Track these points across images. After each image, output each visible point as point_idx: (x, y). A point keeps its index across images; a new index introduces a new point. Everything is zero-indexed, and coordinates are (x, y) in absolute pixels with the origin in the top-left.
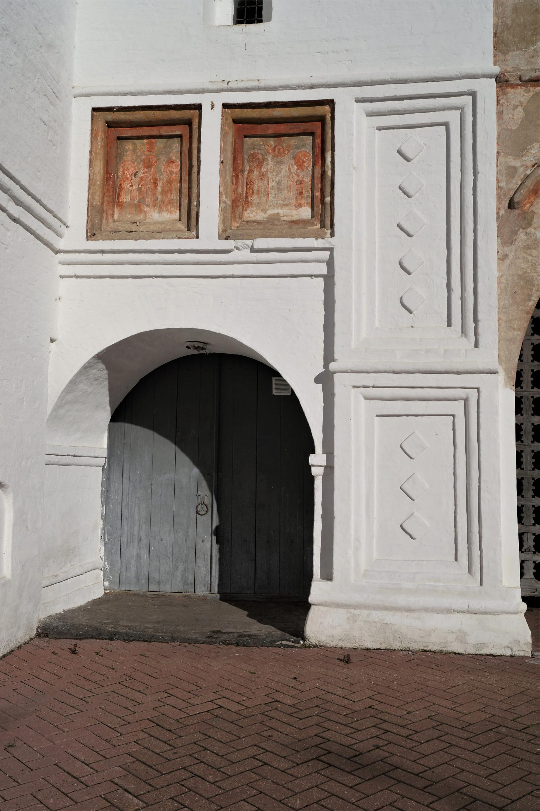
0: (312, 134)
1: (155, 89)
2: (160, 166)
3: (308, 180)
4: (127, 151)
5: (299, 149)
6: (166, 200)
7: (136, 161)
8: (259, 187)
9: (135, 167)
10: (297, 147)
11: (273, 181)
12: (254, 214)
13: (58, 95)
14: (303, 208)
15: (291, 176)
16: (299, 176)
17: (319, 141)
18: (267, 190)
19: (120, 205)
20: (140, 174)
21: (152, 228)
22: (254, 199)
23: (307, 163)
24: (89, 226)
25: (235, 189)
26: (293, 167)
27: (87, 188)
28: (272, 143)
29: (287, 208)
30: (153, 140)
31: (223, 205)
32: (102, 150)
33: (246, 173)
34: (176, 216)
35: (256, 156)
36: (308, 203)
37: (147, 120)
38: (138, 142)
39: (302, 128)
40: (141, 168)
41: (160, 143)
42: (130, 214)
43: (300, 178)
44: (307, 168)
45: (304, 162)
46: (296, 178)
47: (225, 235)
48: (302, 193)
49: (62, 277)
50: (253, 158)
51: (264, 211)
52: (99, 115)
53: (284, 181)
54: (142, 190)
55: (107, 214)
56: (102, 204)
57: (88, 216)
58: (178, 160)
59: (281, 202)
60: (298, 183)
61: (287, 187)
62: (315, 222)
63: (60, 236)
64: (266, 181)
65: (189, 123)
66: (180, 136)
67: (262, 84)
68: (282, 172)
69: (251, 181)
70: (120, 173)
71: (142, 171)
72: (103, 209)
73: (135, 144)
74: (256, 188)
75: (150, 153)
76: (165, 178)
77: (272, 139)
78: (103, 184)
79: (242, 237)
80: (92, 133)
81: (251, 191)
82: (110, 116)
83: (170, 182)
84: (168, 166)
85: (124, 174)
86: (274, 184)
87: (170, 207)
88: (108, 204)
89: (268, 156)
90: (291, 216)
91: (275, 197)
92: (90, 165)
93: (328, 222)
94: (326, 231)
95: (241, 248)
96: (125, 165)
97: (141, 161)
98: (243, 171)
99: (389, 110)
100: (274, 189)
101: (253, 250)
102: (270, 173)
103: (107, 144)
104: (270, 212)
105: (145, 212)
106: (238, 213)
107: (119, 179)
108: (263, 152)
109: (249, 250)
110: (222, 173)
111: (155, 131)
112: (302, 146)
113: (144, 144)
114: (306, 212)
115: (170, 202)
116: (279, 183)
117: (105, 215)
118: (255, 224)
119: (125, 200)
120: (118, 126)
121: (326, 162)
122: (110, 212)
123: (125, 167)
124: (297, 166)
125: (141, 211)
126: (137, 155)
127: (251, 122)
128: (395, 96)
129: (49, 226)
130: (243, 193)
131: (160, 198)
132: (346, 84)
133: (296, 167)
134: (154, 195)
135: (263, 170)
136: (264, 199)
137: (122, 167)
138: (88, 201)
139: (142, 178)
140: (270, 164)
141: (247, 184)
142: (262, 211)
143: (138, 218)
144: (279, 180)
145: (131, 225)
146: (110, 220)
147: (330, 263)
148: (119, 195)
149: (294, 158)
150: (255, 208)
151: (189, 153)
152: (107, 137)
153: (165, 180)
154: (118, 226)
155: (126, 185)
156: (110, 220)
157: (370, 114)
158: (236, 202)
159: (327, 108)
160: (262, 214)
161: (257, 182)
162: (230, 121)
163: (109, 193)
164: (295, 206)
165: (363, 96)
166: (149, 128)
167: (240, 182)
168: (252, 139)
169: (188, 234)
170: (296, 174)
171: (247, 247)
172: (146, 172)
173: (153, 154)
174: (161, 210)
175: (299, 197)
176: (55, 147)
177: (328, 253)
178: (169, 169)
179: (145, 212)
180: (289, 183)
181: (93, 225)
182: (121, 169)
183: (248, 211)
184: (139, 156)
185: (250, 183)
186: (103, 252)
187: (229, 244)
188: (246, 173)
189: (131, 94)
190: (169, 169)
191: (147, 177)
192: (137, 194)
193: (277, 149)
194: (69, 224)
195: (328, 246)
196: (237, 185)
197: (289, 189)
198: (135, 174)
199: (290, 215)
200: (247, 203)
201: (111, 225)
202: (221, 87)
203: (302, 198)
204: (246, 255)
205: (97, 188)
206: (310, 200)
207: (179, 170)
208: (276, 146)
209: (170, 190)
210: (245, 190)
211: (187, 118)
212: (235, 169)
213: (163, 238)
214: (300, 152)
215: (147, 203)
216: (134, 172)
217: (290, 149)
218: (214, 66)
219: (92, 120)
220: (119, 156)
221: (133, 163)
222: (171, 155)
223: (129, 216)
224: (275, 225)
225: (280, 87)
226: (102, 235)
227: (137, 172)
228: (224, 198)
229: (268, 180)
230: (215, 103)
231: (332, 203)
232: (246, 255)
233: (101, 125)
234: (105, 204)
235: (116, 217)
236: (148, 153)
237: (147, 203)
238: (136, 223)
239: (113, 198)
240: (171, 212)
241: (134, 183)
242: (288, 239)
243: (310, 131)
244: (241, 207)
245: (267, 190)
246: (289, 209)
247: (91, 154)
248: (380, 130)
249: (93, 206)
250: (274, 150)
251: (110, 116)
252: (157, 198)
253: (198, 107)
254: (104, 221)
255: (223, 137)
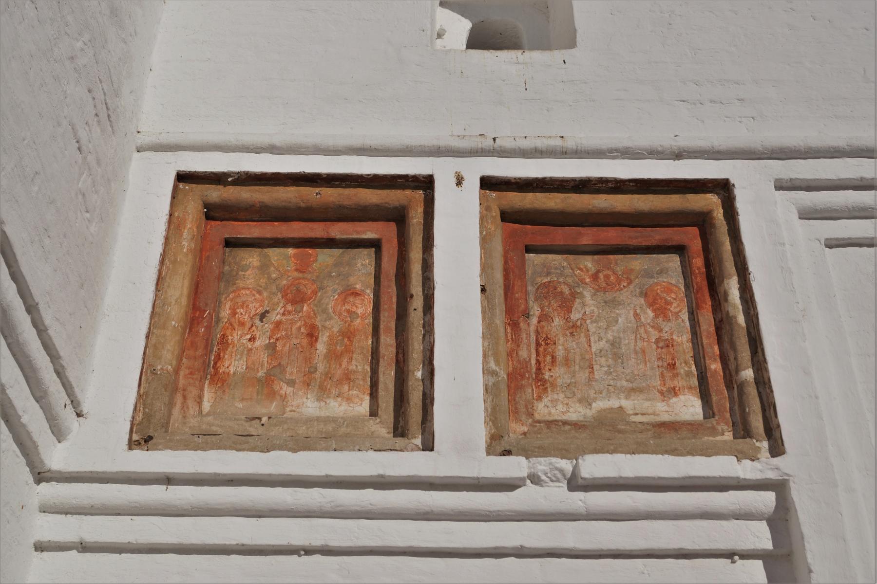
0: (680, 249)
1: (330, 143)
2: (325, 301)
3: (684, 339)
4: (245, 269)
5: (652, 277)
6: (339, 373)
7: (266, 289)
8: (566, 350)
9: (262, 302)
10: (648, 274)
11: (600, 339)
12: (560, 407)
13: (113, 118)
14: (682, 397)
15: (642, 330)
16: (661, 331)
17: (698, 262)
18: (587, 357)
19: (219, 380)
20: (275, 317)
21: (302, 430)
22: (558, 374)
23: (675, 305)
24: (139, 418)
25: (512, 350)
26: (645, 313)
27: (144, 331)
28: (590, 265)
29: (642, 396)
30: (310, 251)
31: (491, 380)
32: (190, 257)
33: (534, 321)
34: (363, 407)
35: (555, 288)
36: (690, 388)
37: (302, 205)
38: (274, 254)
39: (657, 237)
40: (278, 304)
41: (325, 257)
42: (243, 400)
43: (666, 336)
44: (677, 315)
45: (668, 303)
46: (654, 335)
47: (499, 445)
48: (672, 366)
49: (40, 547)
50: (547, 291)
51: (586, 402)
52: (191, 190)
53: (628, 343)
54: (279, 348)
55: (185, 397)
56: (177, 371)
57: (139, 395)
58: (369, 293)
59: (625, 383)
60: (661, 345)
61: (636, 353)
62: (719, 428)
63: (59, 433)
64: (583, 339)
65: (398, 217)
66: (375, 245)
67: (570, 144)
68: (623, 325)
69: (547, 338)
70: (225, 313)
71: (280, 310)
72: (176, 382)
73: (266, 256)
74: (560, 352)
75: (301, 275)
76: (335, 325)
77: (589, 257)
78: (184, 329)
79: (544, 452)
80: (170, 222)
81: (549, 358)
82: (215, 194)
83: (348, 334)
84: (344, 301)
85: (234, 313)
86: (602, 344)
87: (346, 387)
88: (191, 373)
89: (583, 288)
90: (654, 414)
91: (608, 373)
92: (157, 284)
93: (757, 423)
94: (758, 444)
95: (543, 477)
96: (239, 296)
97: (280, 289)
98: (527, 315)
99: (850, 206)
100: (606, 356)
101: (576, 484)
102: (592, 322)
103: (201, 250)
104: (600, 405)
105: (284, 398)
106: (522, 403)
107: (221, 325)
108: (569, 280)
109: (564, 485)
110: (487, 311)
111: (317, 230)
112: (661, 272)
113: (288, 258)
114: (689, 407)
115: (348, 377)
116: (614, 343)
117: (179, 399)
118: (567, 427)
119: (232, 369)
120: (236, 216)
121: (730, 298)
122: (193, 392)
123: (239, 300)
124: (654, 311)
125: (272, 394)
126: (269, 278)
127: (537, 219)
128: (862, 179)
129: (40, 395)
130: (530, 360)
131: (321, 367)
132: (754, 153)
133: (650, 314)
134: (308, 360)
135: (575, 316)
136: (582, 376)
137: (232, 300)
138: (144, 359)
139: (278, 324)
140: (589, 303)
141: (538, 344)
142: (580, 401)
143: (264, 411)
144: (614, 337)
145: (247, 424)
146: (193, 410)
147: (781, 520)
148: (218, 358)
149: (645, 295)
150: (562, 396)
151: (397, 275)
152: (203, 238)
153: (336, 329)
154: (210, 424)
155: (238, 337)
156: (191, 412)
157: (807, 215)
158: (516, 382)
159: (712, 201)
160: (581, 409)
161: (562, 340)
162: (496, 213)
163: (196, 350)
164: (662, 393)
165: (793, 176)
166: (303, 224)
167: (524, 336)
168: (543, 256)
169: (400, 442)
170: (653, 327)
171: (559, 475)
172: (289, 313)
173: (309, 276)
174: (323, 392)
175: (668, 375)
176: (88, 215)
177: (767, 500)
178: (347, 307)
179: (284, 398)
180: (640, 344)
181: (148, 417)
182: (228, 305)
183: (546, 400)
184: (275, 279)
185: (544, 343)
186: (168, 480)
187: (514, 466)
188: (534, 321)
189: (273, 149)
190: (347, 307)
191: (293, 322)
192: (264, 358)
193: (601, 275)
194: (85, 408)
195: (771, 475)
196: (516, 341)
197: (640, 356)
198: (263, 316)
199: (650, 411)
200: (542, 384)
201: (193, 422)
202: (480, 146)
203: (675, 376)
204: (557, 496)
205: (168, 333)
206: (695, 382)
207: (370, 309)
208: (598, 271)
209: (349, 351)
210: (534, 356)
211: (397, 204)
212: (509, 311)
213: (335, 450)
214: (657, 284)
215: (288, 376)
216: (260, 310)
217: (632, 277)
218: (453, 119)
219: (173, 197)
220: (227, 279)
221: (260, 293)
222: (352, 280)
223: (240, 405)
224: (620, 431)
225: (611, 150)
226: (171, 441)
227: (267, 312)
228: (493, 365)
229: (588, 337)
230: (464, 174)
231: (763, 382)
232: (557, 496)
233: (193, 209)
234: (182, 373)
235: (206, 406)
236: (296, 274)
237: (288, 376)
238: (260, 419)
239: (204, 362)
240: (349, 400)
241: (257, 334)
242: (669, 459)
243: (674, 243)
244: (530, 391)
245: (587, 357)
246: (647, 400)
247: (162, 262)
248: (830, 247)
249: (154, 372)
250: (595, 277)
251: (215, 194)
252: (316, 368)
253: (426, 184)
254: (176, 411)
255: (485, 240)
